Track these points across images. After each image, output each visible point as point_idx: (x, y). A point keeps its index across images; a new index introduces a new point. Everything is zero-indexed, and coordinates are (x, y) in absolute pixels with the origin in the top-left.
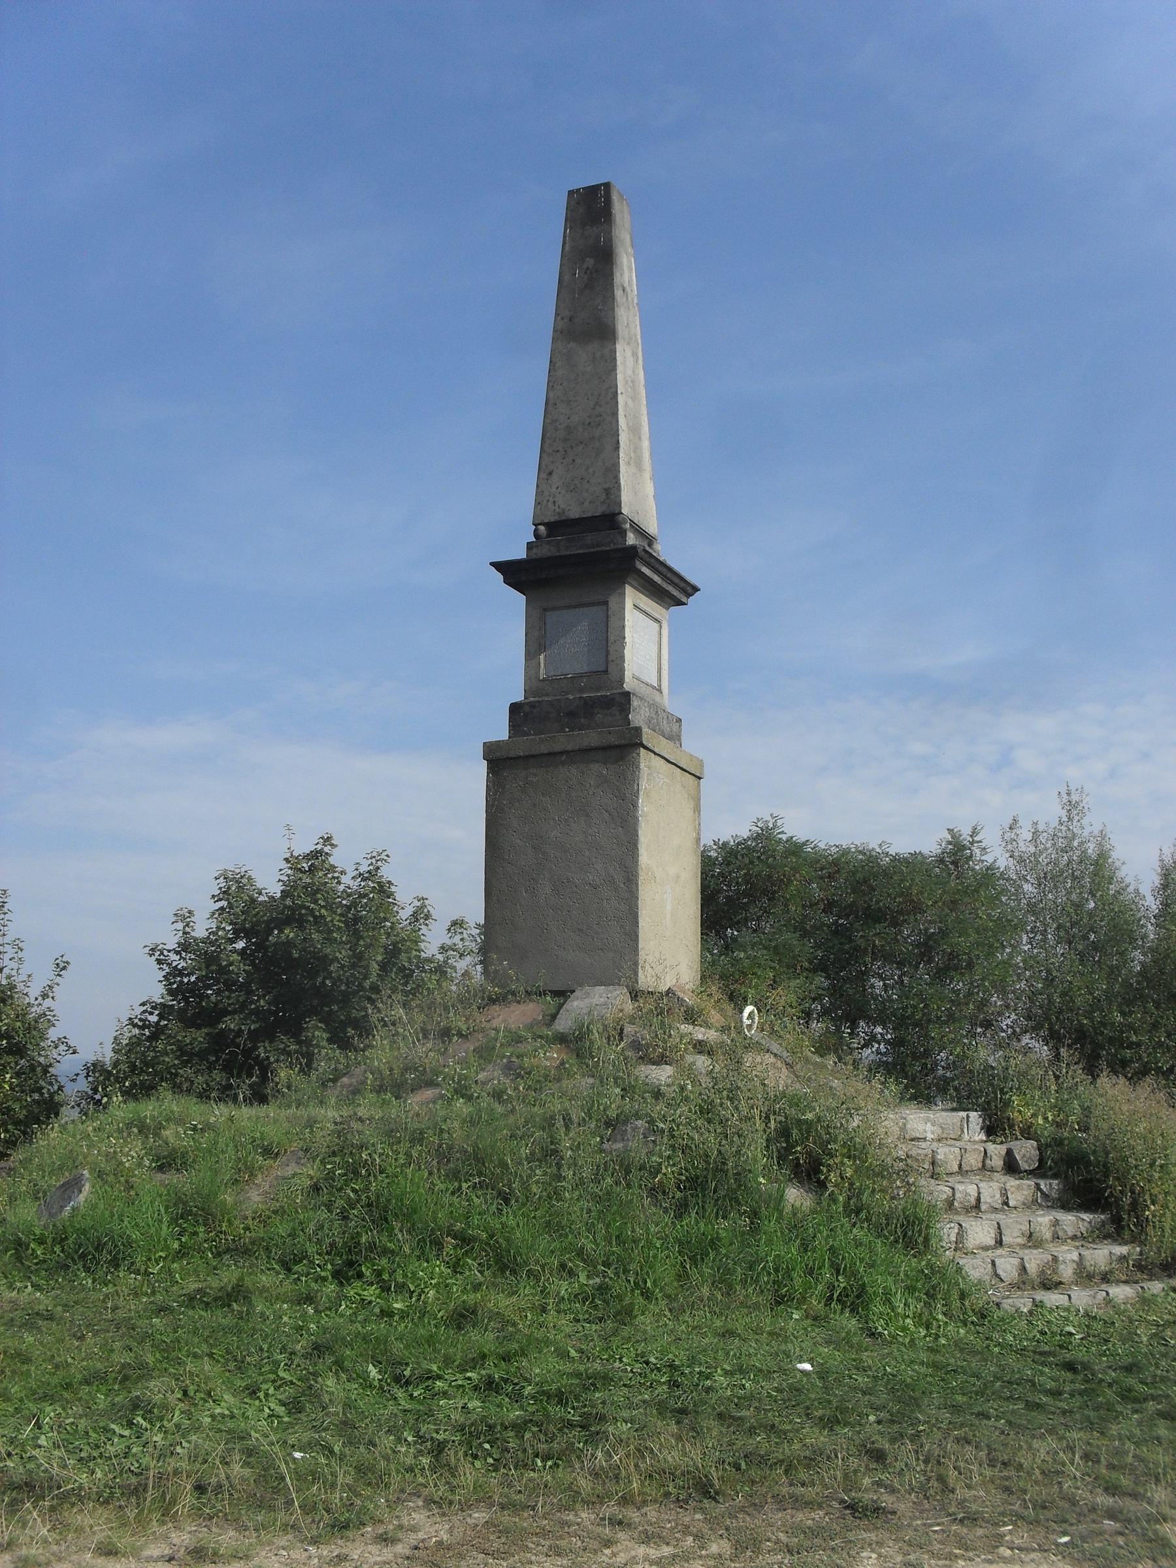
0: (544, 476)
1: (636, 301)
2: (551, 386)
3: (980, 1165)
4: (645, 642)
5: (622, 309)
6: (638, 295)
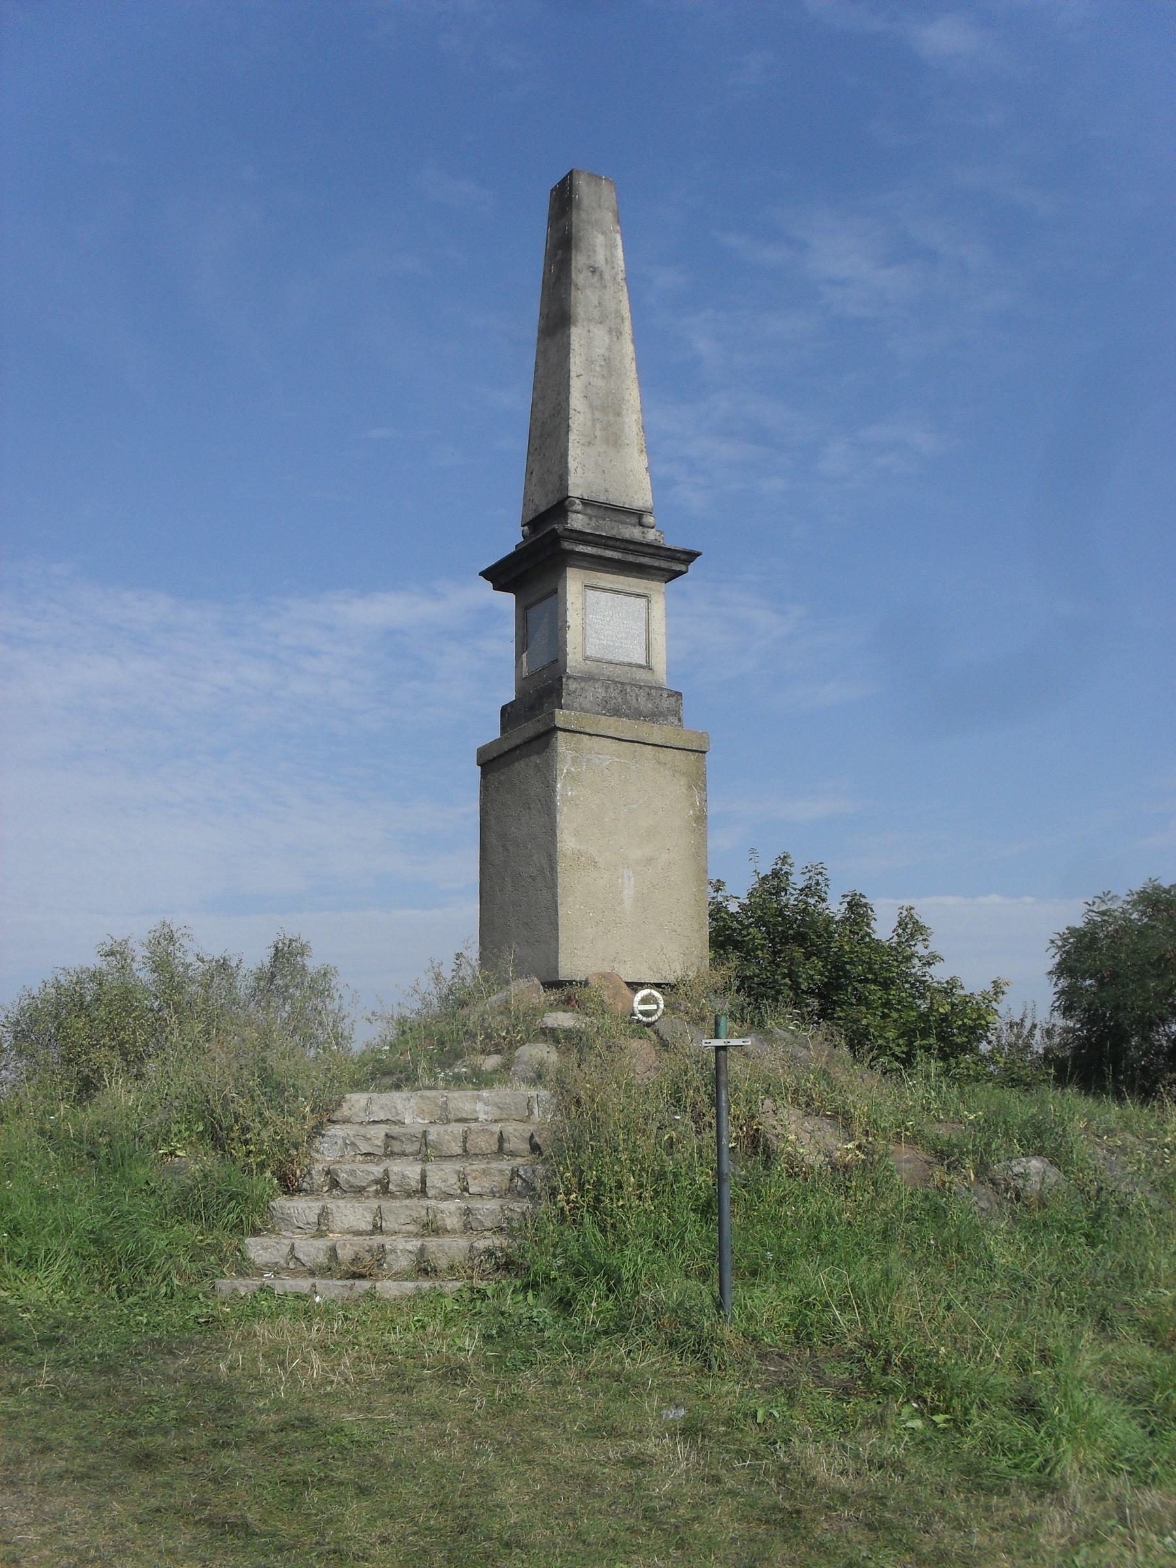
1: (621, 276)
3: (495, 1148)
5: (588, 292)
6: (627, 271)
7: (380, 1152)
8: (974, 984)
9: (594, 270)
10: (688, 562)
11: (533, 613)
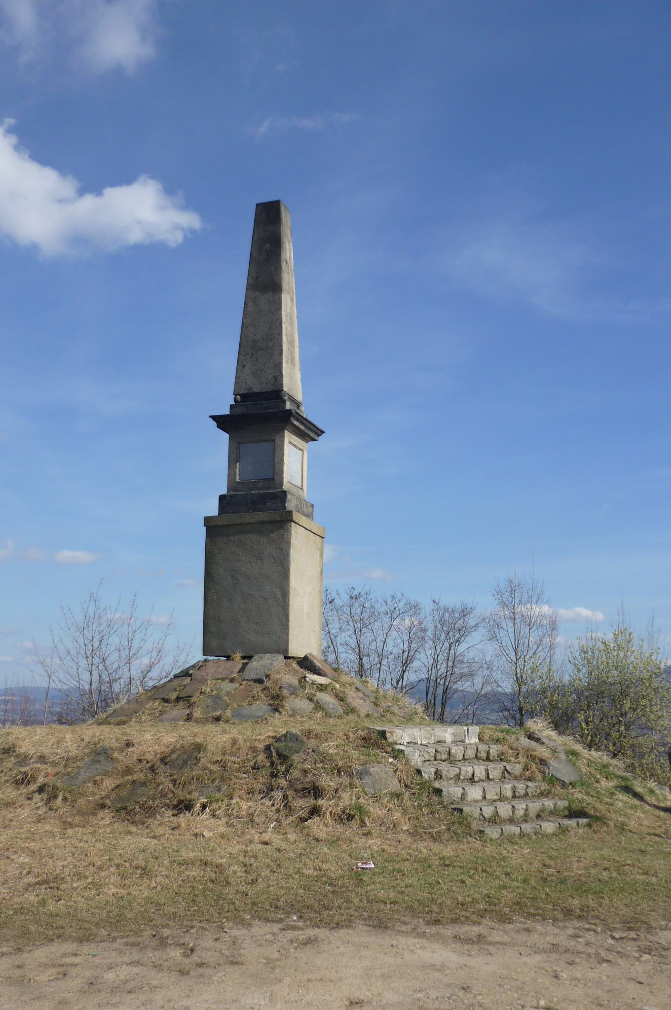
0: (240, 367)
2: (244, 317)
4: (295, 461)
10: (319, 435)
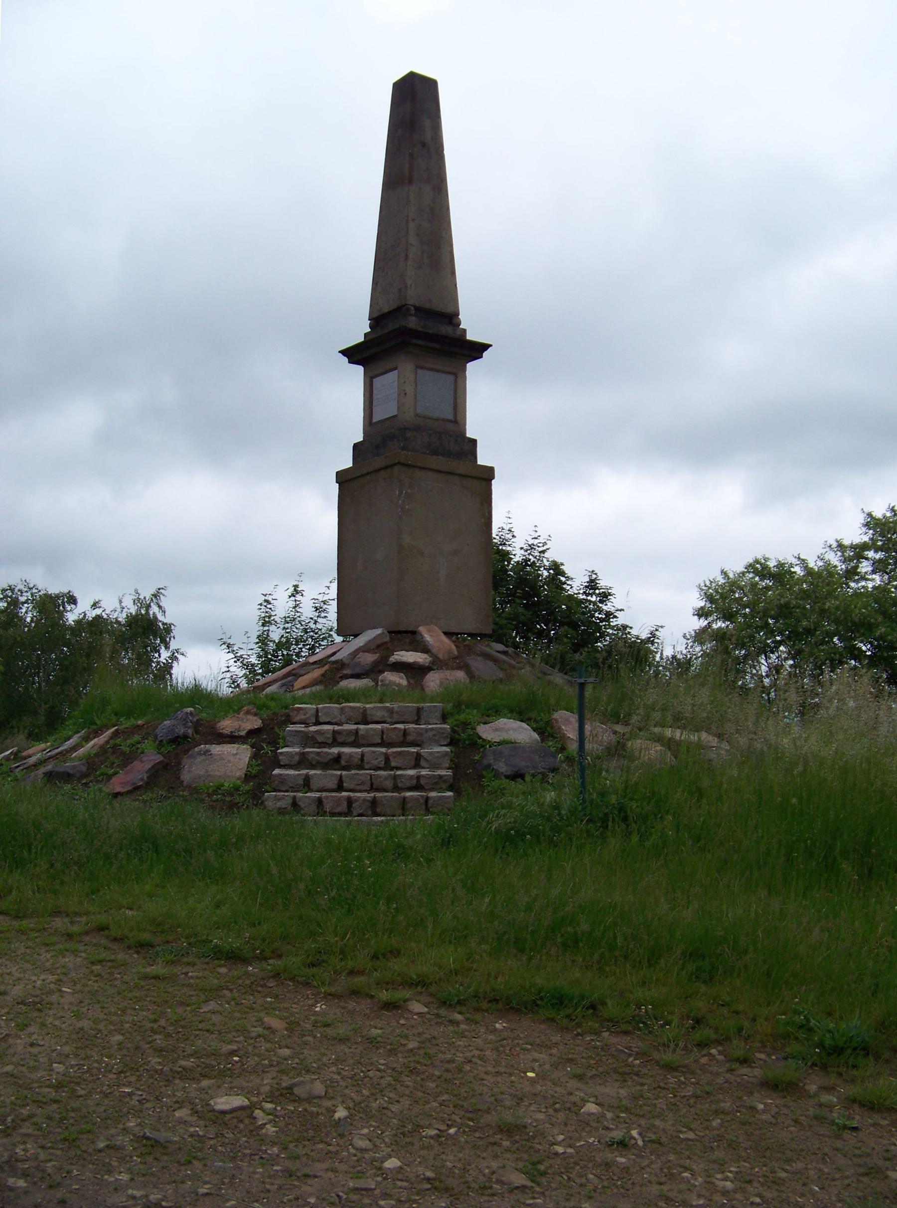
7: (330, 741)
8: (640, 630)
9: (424, 145)
11: (377, 381)
